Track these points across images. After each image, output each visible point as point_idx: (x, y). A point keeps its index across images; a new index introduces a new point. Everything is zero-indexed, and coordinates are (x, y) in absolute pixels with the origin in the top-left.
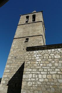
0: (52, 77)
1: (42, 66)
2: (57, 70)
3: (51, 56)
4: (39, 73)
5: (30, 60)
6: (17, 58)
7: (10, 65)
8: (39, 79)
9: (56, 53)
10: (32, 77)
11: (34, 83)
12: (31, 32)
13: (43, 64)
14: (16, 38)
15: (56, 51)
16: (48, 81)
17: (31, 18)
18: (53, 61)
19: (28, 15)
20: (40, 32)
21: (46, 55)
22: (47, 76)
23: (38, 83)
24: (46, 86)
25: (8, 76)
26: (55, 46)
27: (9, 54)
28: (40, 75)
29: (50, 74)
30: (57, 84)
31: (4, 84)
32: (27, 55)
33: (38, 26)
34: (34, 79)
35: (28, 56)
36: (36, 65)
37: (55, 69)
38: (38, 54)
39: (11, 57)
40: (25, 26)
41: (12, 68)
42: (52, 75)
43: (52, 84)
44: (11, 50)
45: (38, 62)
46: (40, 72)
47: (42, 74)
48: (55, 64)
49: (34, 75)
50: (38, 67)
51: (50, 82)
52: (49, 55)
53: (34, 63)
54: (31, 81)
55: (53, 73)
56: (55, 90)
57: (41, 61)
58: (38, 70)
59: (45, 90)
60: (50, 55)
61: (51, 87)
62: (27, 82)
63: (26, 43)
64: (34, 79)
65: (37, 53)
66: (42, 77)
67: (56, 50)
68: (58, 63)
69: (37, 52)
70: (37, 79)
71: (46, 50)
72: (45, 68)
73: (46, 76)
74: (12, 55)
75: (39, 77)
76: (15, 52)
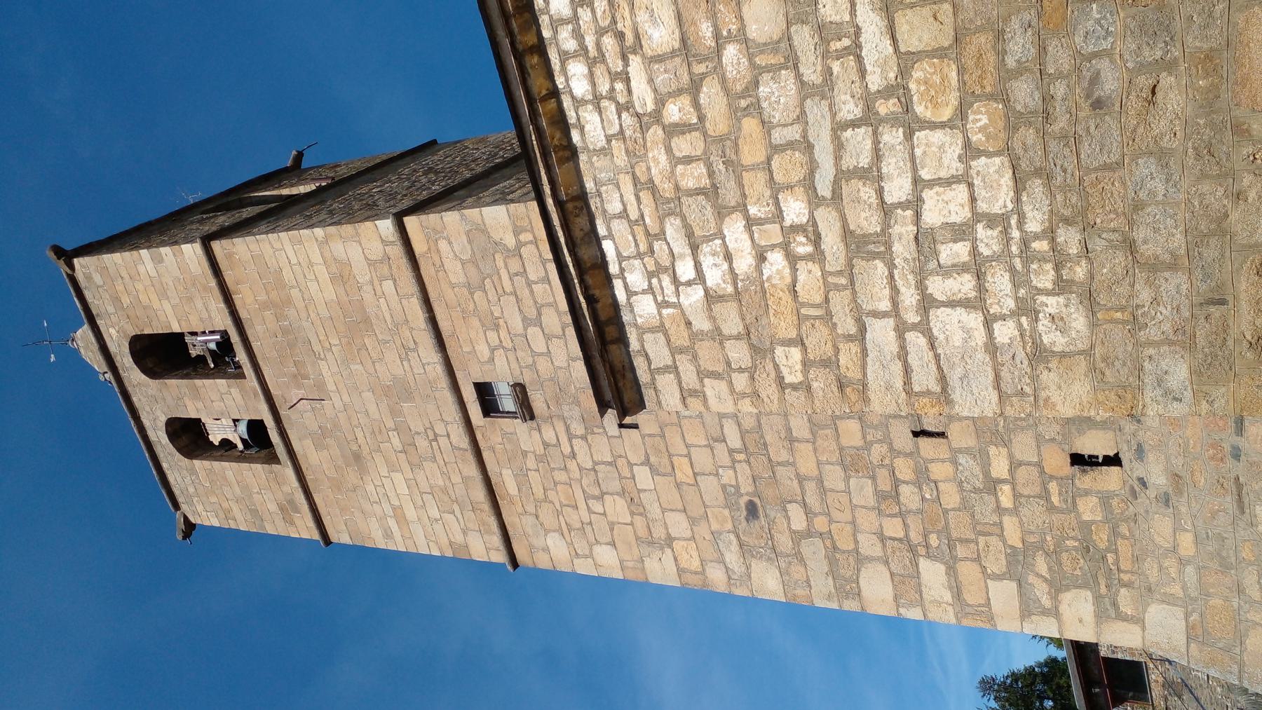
0: (939, 53)
1: (815, 201)
3: (661, 102)
4: (903, 229)
5: (761, 351)
6: (746, 487)
7: (861, 560)
8: (977, 217)
9: (609, 42)
10: (965, 304)
11: (1044, 278)
12: (391, 366)
13: (776, 190)
14: (496, 540)
15: (578, 35)
16: (991, 97)
17: (196, 395)
18: (719, 69)
19: (159, 437)
21: (658, 161)
22: (933, 126)
23: (1033, 226)
25: (996, 564)
27: (728, 598)
28: (932, 216)
29: (898, 90)
31: (1098, 598)
32: (699, 394)
33: (281, 284)
34: (1000, 282)
35: (713, 389)
36: (809, 276)
37: (824, 32)
39: (758, 567)
41: (893, 528)
42: (906, 61)
43: (1019, 47)
44: (661, 570)
45: (761, 258)
46: (886, 210)
48: (753, 31)
49: (938, 287)
51: (1007, 75)
52: (656, 133)
54: (1026, 309)
55: (875, 44)
57: (750, 223)
58: (865, 239)
60: (657, 116)
61: (1059, 60)
62: (1039, 355)
63: (538, 402)
64: (1000, 282)
65: (650, 275)
66: (949, 182)
70: (988, 240)
71: (593, 172)
72: (824, 154)
73: (937, 136)
74: (732, 557)
75: (960, 214)
76: (678, 525)
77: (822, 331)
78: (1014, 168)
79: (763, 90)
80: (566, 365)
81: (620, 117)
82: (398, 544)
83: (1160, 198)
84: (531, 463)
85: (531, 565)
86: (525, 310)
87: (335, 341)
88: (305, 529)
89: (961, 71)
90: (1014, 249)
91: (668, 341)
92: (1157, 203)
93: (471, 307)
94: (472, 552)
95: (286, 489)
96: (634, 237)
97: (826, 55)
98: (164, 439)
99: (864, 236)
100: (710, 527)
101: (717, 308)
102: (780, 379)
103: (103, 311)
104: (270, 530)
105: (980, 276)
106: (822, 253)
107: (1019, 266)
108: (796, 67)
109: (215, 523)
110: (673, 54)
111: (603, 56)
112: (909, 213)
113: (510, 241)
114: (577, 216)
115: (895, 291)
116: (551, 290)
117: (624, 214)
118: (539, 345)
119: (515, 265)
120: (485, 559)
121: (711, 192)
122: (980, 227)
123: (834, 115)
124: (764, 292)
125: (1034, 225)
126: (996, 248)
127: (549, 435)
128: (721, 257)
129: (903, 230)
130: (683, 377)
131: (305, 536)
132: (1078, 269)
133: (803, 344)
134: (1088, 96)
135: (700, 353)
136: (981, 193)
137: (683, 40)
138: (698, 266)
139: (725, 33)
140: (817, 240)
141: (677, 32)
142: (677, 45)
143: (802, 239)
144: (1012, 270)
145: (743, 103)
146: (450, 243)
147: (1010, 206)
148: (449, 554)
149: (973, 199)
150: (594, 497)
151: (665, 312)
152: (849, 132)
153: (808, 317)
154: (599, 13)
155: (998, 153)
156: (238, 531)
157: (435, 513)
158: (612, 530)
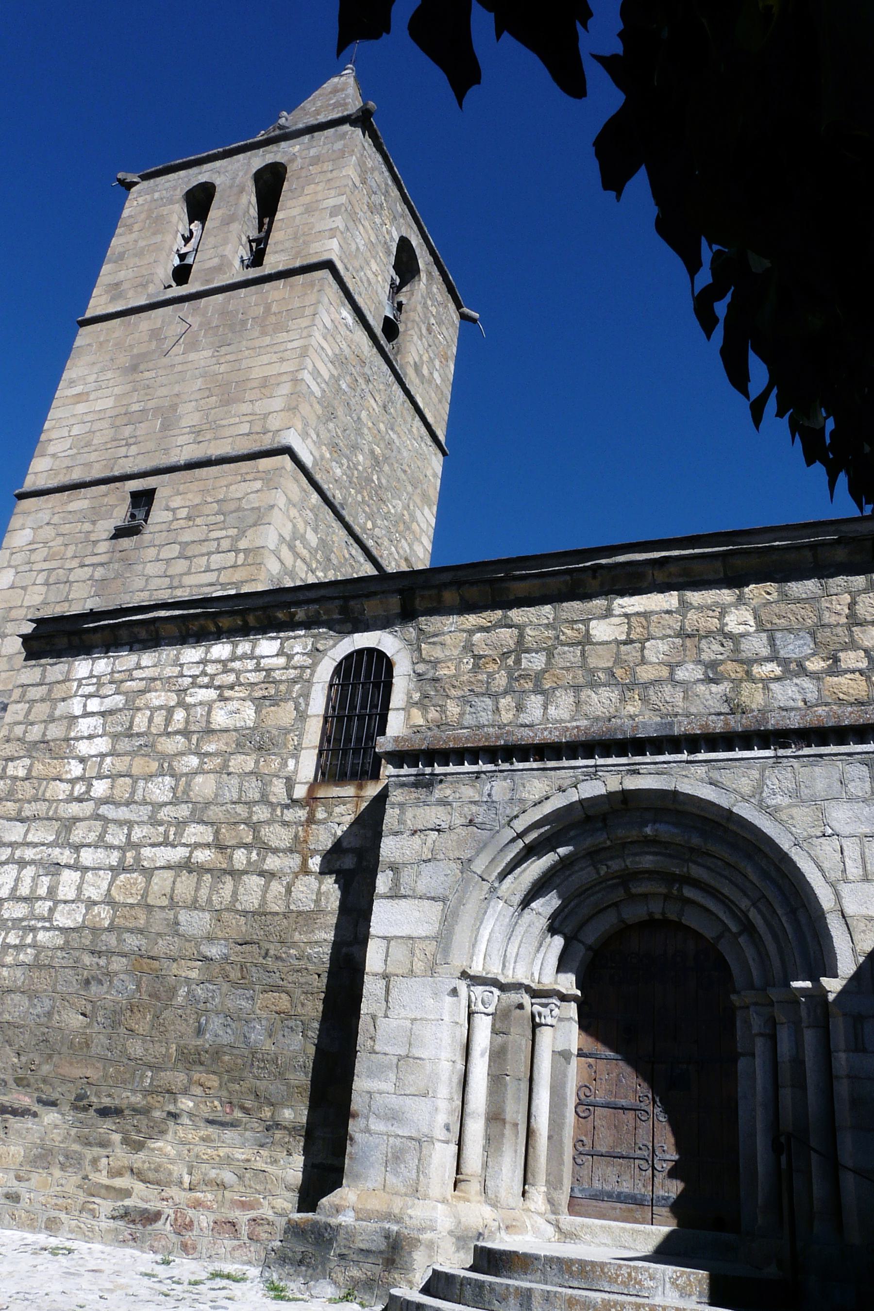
0: (145, 895)
1: (106, 801)
2: (196, 833)
4: (65, 856)
9: (231, 678)
10: (14, 889)
12: (190, 417)
15: (244, 657)
20: (277, 403)
22: (111, 884)
24: (87, 959)
26: (243, 613)
30: (162, 947)
33: (281, 328)
38: (100, 685)
40: (155, 334)
42: (148, 873)
43: (133, 942)
45: (82, 760)
47: (85, 869)
50: (74, 809)
53: (54, 767)
56: (138, 986)
57: (103, 756)
59: (75, 987)
60: (181, 704)
61: (118, 964)
63: (125, 543)
66: (79, 889)
67: (244, 647)
68: (224, 770)
69: (102, 665)
77: (30, 792)
78: (73, 929)
79: (167, 779)
80: (145, 573)
81: (190, 676)
82: (63, 391)
83: (31, 1010)
84: (87, 526)
85: (16, 510)
86: (193, 546)
87: (222, 369)
88: (98, 304)
89: (132, 906)
90: (33, 922)
91: (58, 682)
92: (29, 1009)
93: (209, 500)
94: (38, 459)
95: (130, 294)
96: (123, 671)
97: (170, 824)
98: (203, 179)
99: (70, 831)
100: (4, 671)
101: (65, 722)
102: (12, 759)
103: (314, 144)
104: (105, 269)
105: (25, 899)
106: (71, 802)
107: (24, 923)
108: (171, 803)
109: (126, 213)
110: (208, 722)
111: (226, 672)
112: (72, 862)
113: (243, 544)
114: (147, 632)
115: (35, 845)
116: (200, 572)
117: (138, 667)
118: (166, 553)
119: (225, 544)
120: (30, 470)
121: (129, 734)
122: (51, 904)
123: (137, 823)
124: (62, 758)
125: (42, 936)
126: (37, 911)
127: (103, 547)
128: (92, 733)
129: (65, 857)
130: (35, 688)
131: (92, 302)
132: (11, 958)
133: (27, 779)
134: (93, 977)
135: (44, 705)
136: (67, 907)
137: (213, 731)
138: (92, 714)
139: (206, 760)
140: (80, 800)
141: (218, 727)
142: (212, 726)
143: (84, 789)
144: (21, 920)
145: (166, 765)
146: (257, 491)
147: (55, 923)
148: (43, 437)
149: (65, 902)
150: (48, 577)
151: (75, 684)
152: (126, 831)
153: (40, 785)
154: (248, 675)
155: (84, 921)
156: (112, 235)
157: (75, 431)
158: (22, 588)
